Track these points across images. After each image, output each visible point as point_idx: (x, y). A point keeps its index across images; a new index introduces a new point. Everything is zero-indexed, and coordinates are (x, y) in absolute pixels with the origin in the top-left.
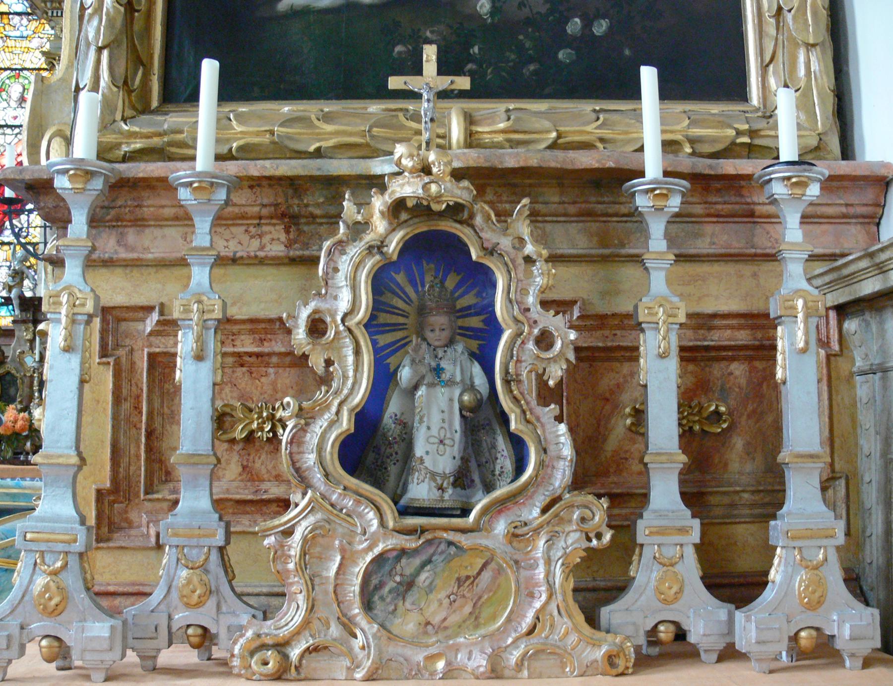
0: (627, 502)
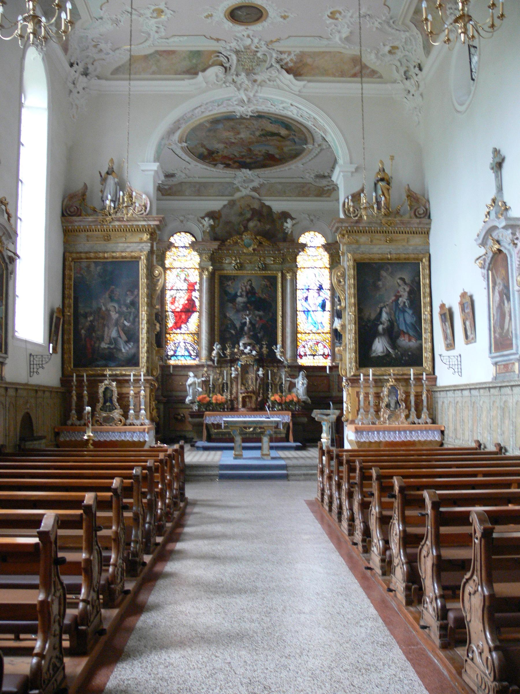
0: (410, 410)
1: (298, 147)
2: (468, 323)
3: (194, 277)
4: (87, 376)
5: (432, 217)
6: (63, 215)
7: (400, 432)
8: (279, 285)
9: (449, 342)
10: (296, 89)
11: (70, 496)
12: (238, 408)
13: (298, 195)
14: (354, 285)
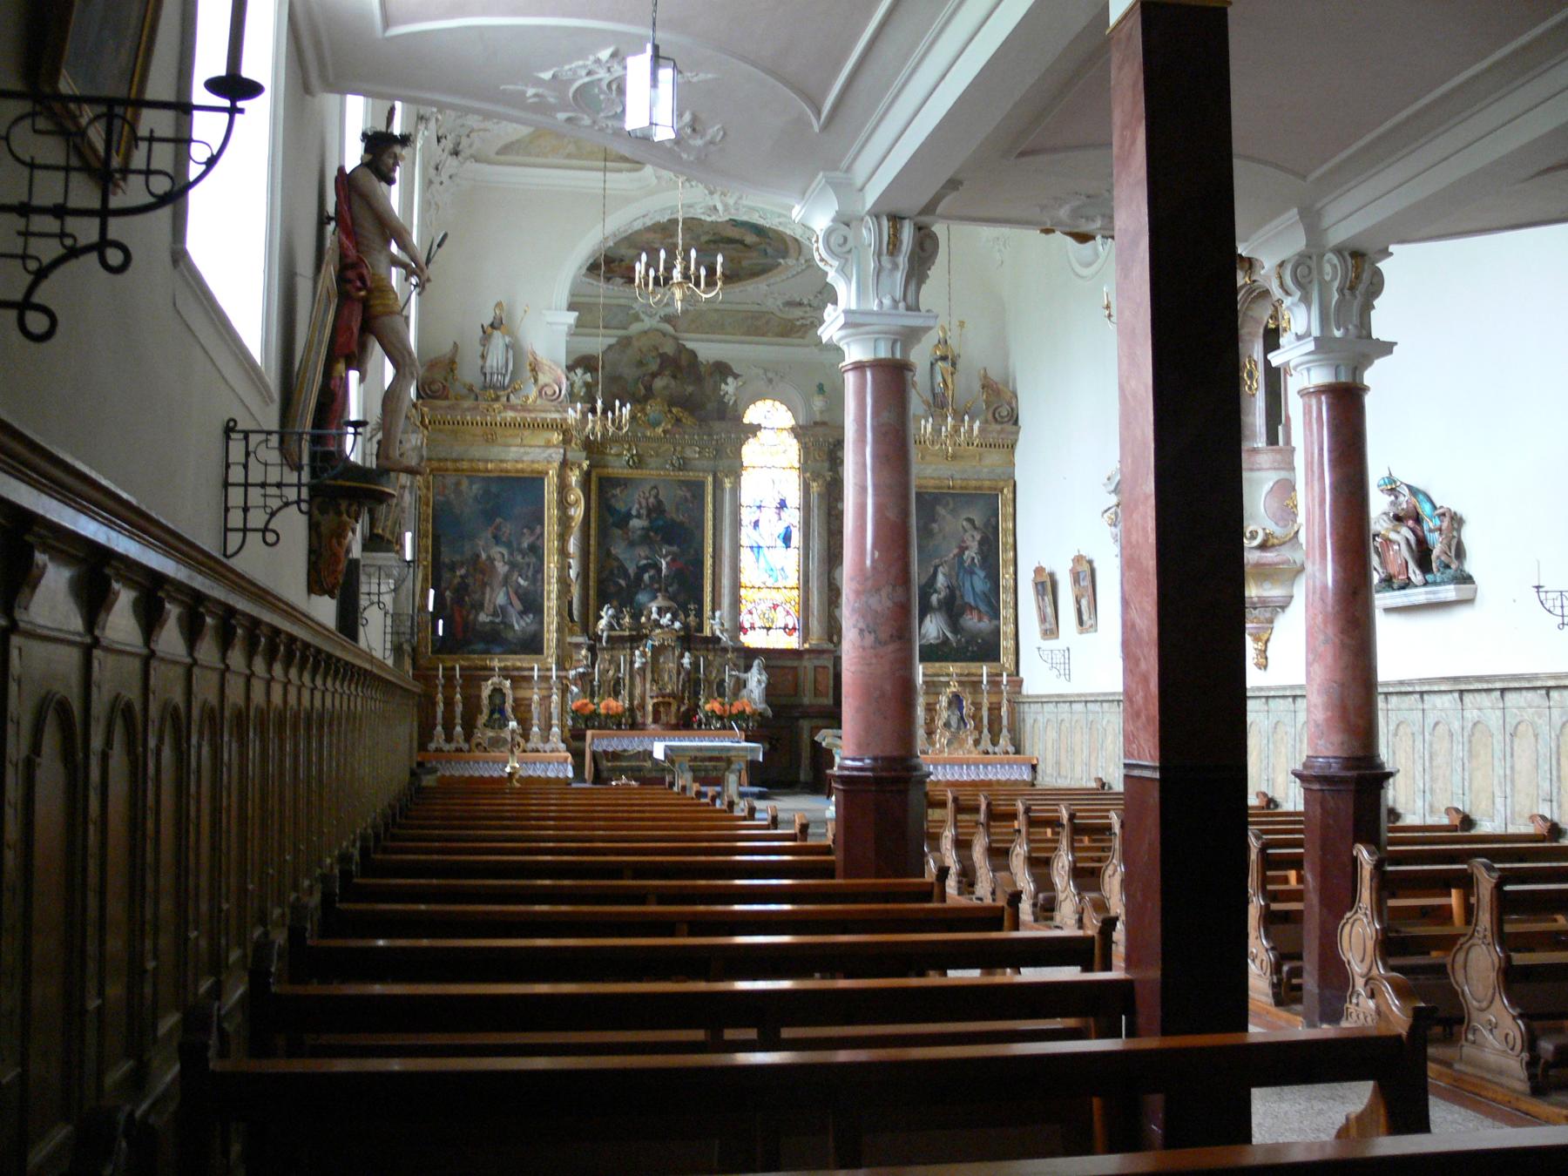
1: (769, 261)
2: (1084, 602)
4: (461, 668)
5: (1020, 422)
7: (961, 766)
8: (709, 499)
9: (1048, 626)
12: (644, 724)
13: (748, 333)
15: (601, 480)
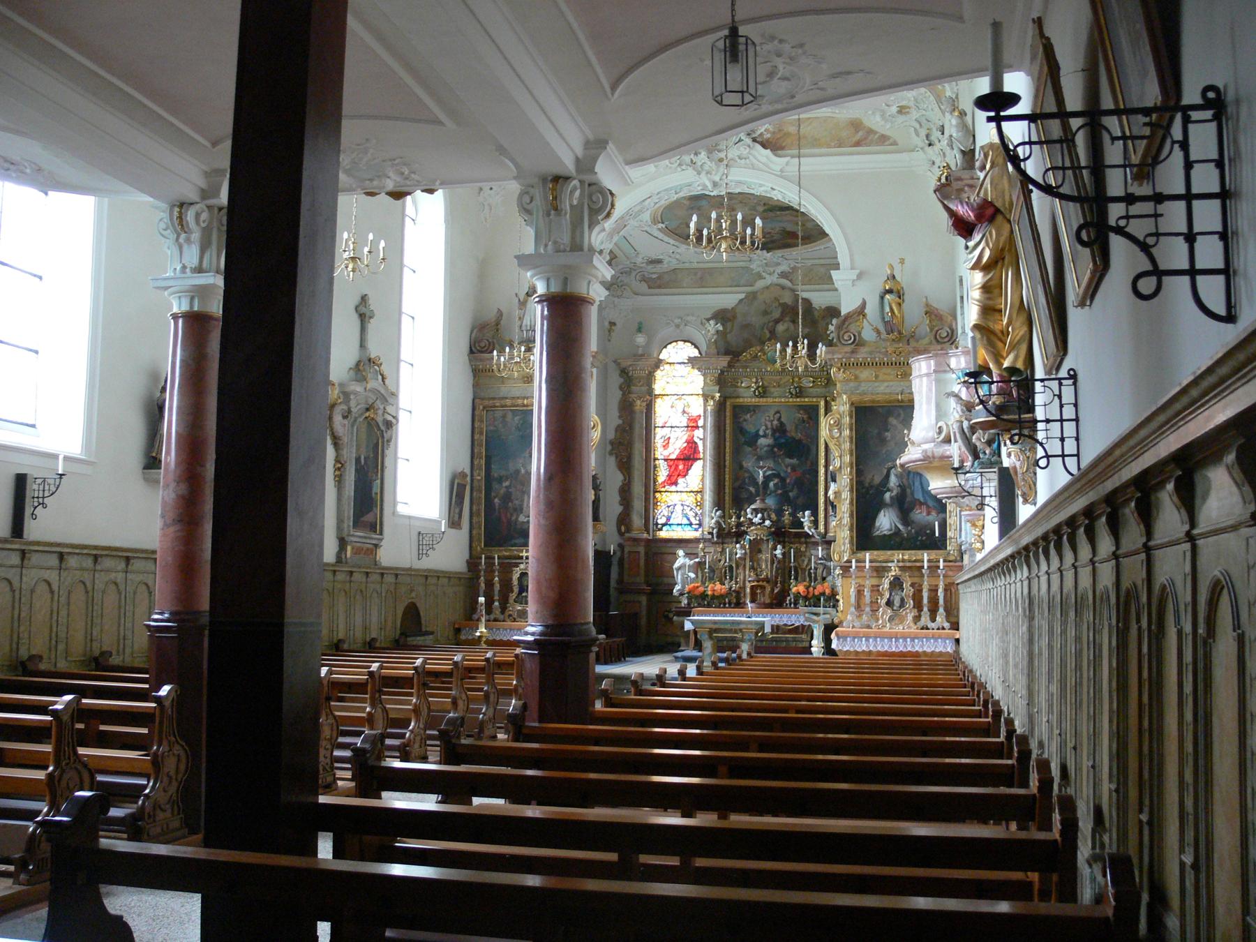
3: (696, 407)
6: (471, 352)
7: (897, 639)
10: (778, 168)
11: (802, 825)
14: (851, 438)
15: (735, 407)
